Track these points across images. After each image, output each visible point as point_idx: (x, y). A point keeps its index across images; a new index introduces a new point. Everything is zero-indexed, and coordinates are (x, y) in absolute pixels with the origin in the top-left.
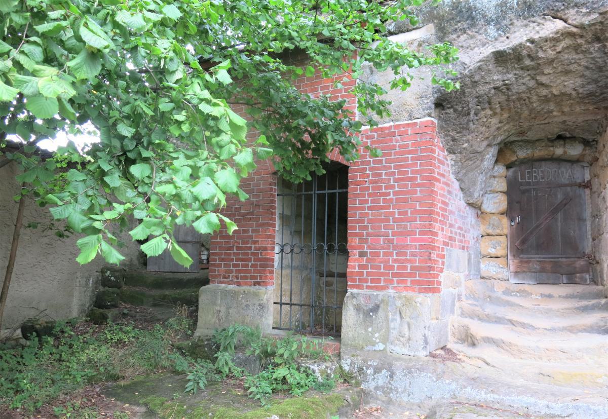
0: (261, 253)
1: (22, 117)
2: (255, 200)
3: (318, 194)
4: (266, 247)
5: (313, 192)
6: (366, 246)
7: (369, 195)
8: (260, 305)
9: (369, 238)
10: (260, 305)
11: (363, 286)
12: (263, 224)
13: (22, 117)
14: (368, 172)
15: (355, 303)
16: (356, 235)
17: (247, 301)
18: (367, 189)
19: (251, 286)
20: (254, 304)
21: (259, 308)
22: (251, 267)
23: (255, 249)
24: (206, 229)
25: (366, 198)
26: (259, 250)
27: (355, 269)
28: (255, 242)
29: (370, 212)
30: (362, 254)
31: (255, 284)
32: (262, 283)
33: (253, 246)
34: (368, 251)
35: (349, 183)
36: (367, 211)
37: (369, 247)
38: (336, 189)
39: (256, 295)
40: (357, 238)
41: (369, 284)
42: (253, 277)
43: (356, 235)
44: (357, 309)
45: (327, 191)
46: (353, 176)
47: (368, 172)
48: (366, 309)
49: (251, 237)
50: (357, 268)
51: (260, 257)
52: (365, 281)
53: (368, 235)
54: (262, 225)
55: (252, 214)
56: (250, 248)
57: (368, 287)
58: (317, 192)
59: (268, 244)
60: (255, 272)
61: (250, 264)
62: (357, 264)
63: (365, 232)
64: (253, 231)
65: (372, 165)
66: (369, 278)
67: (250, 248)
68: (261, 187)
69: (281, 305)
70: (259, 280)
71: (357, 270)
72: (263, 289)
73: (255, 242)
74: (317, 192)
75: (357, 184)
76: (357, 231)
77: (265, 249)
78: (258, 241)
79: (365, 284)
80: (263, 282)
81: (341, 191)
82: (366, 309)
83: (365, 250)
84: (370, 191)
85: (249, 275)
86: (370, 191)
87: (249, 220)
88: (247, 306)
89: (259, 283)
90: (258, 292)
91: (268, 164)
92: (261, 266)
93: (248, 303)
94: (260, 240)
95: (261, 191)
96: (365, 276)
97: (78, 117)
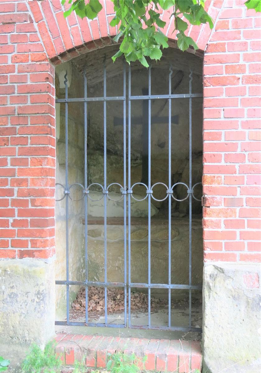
0: (33, 201)
1: (185, 300)
2: (16, 106)
3: (132, 101)
4: (42, 190)
5: (124, 98)
6: (239, 189)
7: (245, 102)
8: (38, 293)
9: (245, 176)
10: (38, 293)
11: (234, 256)
12: (36, 150)
13: (185, 300)
14: (241, 62)
15: (230, 287)
16: (220, 170)
17: (12, 287)
18: (242, 92)
19: (14, 258)
20: (27, 293)
21: (36, 300)
22: (13, 225)
23: (20, 193)
24: (73, 278)
25: (240, 107)
26: (29, 195)
27: (220, 227)
28: (20, 182)
29: (247, 131)
30: (231, 203)
31: (22, 255)
32: (36, 254)
33: (16, 189)
34: (244, 197)
35: (205, 81)
36: (240, 129)
37: (244, 191)
38: (168, 93)
39: (29, 275)
40: (223, 176)
41: (246, 252)
42: (15, 244)
43: (220, 170)
44: (234, 297)
45: (150, 97)
46: (209, 69)
47: (241, 62)
48: (251, 296)
49: (11, 173)
50: (223, 225)
51: (30, 207)
52: (240, 247)
53: (243, 170)
54: (33, 152)
55: (12, 131)
56: (10, 193)
57: (244, 258)
58: (131, 98)
59: (46, 185)
60: (20, 233)
61: (11, 220)
62: (223, 219)
63: (237, 166)
64: (15, 162)
65: (250, 51)
66: (246, 242)
67: (10, 193)
68: (29, 83)
69: (68, 285)
70: (30, 248)
71: (223, 228)
72: (39, 262)
73: (20, 182)
74: (131, 98)
75: (220, 82)
76: (223, 163)
77: (42, 193)
78: (26, 180)
79: (238, 253)
80: (40, 251)
81: (176, 96)
82: (251, 296)
83: (238, 196)
84: (247, 96)
85: (10, 239)
86: (247, 96)
87: (6, 142)
88: (13, 296)
89: (30, 254)
90: (35, 272)
91: (41, 42)
92: (33, 224)
93: (14, 291)
94: (29, 178)
95: (30, 90)
96: (238, 239)
97: (121, 316)
